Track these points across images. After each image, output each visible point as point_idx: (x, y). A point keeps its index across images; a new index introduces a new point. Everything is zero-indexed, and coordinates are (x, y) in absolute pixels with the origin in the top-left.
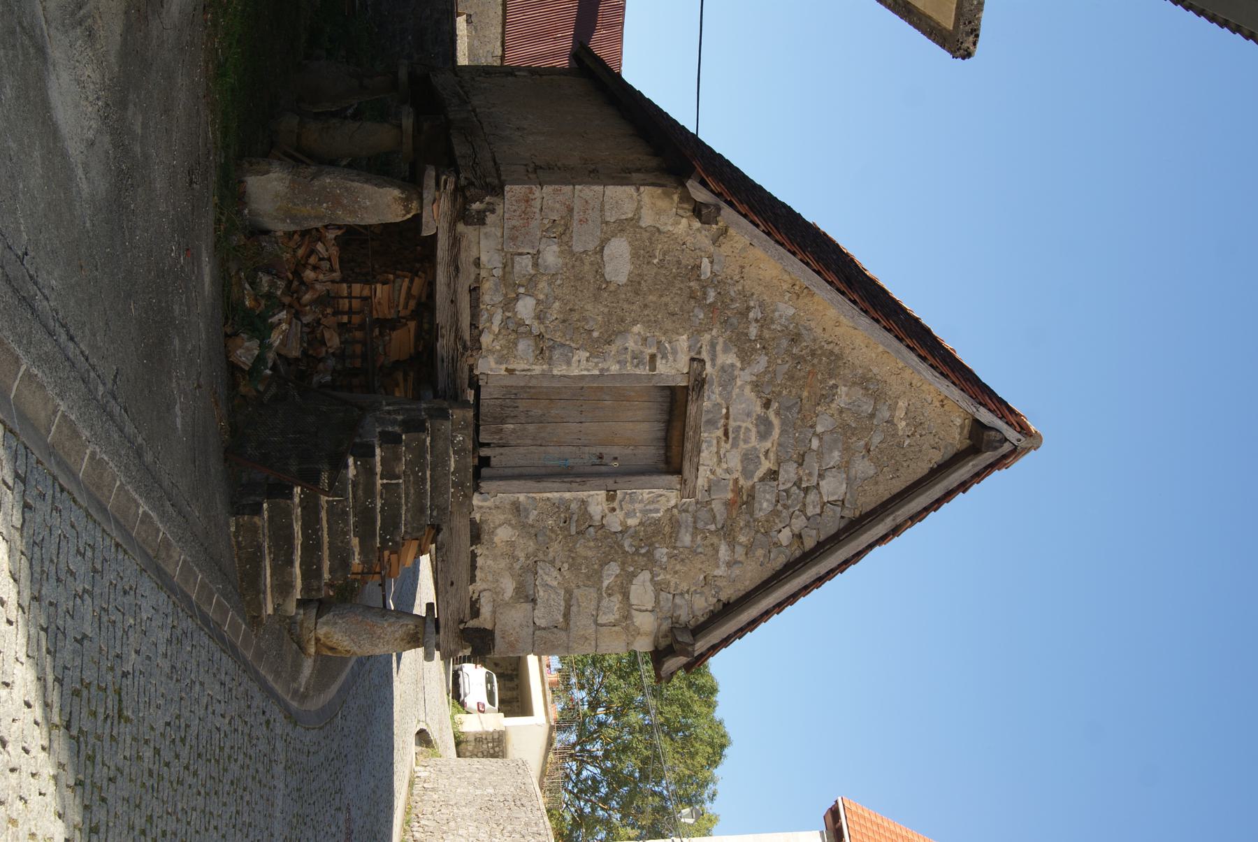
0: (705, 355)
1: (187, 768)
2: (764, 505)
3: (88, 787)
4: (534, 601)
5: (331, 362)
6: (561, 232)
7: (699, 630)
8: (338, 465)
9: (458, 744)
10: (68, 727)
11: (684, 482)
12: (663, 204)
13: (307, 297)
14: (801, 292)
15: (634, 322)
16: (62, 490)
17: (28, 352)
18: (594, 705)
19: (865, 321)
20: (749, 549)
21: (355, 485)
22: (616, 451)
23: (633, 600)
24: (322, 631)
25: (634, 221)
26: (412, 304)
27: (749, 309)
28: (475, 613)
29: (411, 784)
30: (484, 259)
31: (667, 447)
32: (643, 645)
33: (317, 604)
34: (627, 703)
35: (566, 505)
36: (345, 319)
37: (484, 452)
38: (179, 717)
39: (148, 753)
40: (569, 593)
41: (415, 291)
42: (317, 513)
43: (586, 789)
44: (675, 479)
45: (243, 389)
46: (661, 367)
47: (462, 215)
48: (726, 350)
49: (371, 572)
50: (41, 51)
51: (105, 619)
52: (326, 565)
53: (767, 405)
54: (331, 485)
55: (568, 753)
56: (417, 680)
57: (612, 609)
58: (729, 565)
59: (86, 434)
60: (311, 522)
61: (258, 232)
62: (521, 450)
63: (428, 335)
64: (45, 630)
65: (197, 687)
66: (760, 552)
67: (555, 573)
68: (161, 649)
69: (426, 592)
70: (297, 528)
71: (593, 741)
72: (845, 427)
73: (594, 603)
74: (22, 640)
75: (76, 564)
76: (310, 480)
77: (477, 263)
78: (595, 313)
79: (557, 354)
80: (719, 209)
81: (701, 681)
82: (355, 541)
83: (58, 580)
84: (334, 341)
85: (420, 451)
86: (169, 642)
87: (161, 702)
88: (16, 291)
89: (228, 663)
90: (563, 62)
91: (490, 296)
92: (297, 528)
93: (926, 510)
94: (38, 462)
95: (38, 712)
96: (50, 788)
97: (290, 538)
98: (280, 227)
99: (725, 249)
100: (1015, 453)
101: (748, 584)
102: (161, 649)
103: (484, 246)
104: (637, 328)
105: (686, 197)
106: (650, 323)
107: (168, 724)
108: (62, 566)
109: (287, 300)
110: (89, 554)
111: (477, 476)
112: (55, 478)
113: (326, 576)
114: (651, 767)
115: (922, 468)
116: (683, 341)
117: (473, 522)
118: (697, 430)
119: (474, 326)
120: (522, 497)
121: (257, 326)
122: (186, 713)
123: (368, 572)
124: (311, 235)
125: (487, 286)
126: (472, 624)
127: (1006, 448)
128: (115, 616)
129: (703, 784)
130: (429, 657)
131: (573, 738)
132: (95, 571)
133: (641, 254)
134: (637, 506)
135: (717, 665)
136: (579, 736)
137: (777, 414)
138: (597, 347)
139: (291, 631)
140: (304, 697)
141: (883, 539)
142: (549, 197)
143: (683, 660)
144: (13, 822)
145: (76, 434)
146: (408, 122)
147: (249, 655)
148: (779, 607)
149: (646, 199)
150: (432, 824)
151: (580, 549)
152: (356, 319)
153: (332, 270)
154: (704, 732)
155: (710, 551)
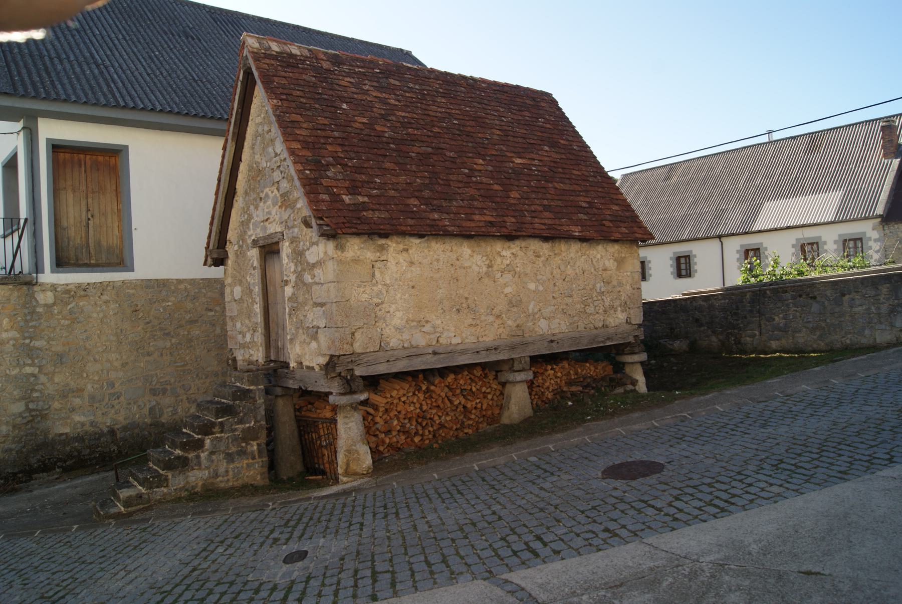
35: (290, 310)
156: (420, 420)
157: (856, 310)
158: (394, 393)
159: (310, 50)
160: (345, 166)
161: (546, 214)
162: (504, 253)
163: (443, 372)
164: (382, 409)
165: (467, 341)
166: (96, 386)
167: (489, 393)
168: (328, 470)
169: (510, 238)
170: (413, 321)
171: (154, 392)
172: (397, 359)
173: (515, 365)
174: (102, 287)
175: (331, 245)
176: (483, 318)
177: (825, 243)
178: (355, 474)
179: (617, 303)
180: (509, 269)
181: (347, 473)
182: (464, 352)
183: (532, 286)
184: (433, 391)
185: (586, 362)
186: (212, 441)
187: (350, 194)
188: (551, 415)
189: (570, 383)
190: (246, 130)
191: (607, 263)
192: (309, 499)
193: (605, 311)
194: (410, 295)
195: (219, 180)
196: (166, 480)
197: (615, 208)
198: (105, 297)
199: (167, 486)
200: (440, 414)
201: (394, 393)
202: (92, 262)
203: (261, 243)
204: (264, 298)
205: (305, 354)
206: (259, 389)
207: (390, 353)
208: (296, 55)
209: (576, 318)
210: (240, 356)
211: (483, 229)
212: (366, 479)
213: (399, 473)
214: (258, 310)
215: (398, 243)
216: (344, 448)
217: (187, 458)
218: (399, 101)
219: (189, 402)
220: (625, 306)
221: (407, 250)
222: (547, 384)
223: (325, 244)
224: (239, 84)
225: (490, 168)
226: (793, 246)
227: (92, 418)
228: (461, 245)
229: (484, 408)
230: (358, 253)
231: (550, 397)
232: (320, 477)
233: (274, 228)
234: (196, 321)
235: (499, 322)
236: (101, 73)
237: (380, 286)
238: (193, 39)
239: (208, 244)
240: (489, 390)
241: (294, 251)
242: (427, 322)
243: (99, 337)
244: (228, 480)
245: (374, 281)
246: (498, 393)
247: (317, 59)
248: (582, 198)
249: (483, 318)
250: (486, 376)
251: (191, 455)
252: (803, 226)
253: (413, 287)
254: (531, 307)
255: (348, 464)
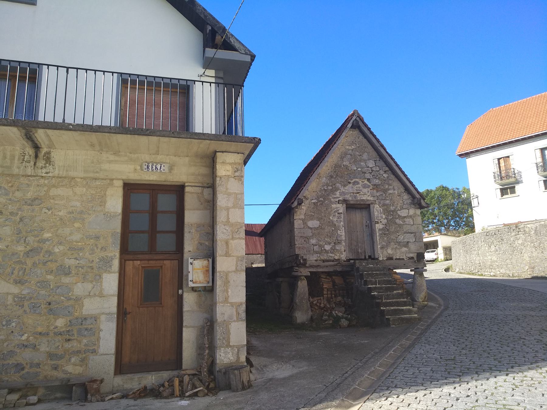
0: (337, 200)
1: (466, 340)
2: (377, 181)
3: (479, 370)
4: (408, 242)
5: (345, 299)
6: (307, 239)
7: (413, 197)
8: (374, 297)
9: (448, 260)
10: (460, 376)
11: (372, 203)
12: (298, 213)
13: (328, 306)
14: (319, 177)
15: (330, 219)
16: (389, 376)
17: (352, 385)
18: (433, 223)
19: (326, 159)
20: (389, 185)
21: (379, 293)
22: (364, 222)
23: (406, 215)
24: (420, 300)
25: (303, 220)
26: (328, 277)
27: (324, 189)
28: (412, 258)
29: (461, 273)
30: (315, 259)
31: (363, 208)
32: (418, 212)
33: (413, 301)
34: (432, 214)
35: (380, 234)
36: (333, 295)
37: (367, 257)
38: (451, 342)
39: (464, 351)
40: (405, 233)
41: (324, 277)
42: (388, 302)
43: (458, 224)
44: (371, 206)
45: (355, 323)
46: (341, 211)
47: (304, 265)
48: (335, 195)
49: (403, 287)
50: (271, 380)
51: (425, 364)
52: (402, 300)
53: (350, 183)
54: (380, 299)
55: (447, 229)
56: (433, 272)
57: (409, 221)
58: (394, 190)
59: (373, 369)
60: (391, 304)
61: (312, 319)
62: (366, 247)
63: (336, 273)
64: (431, 382)
65: (442, 336)
66: (390, 182)
67: (400, 237)
68: (432, 347)
69: (407, 271)
70: (392, 308)
71: (443, 223)
72: (354, 162)
73: (408, 226)
74: (436, 389)
75: (411, 372)
76: (379, 305)
77: (316, 260)
78: (327, 229)
79: (339, 239)
80: (299, 199)
81: (425, 194)
82: (395, 292)
83: (416, 378)
84: (339, 299)
85: (369, 275)
86: (429, 345)
87: (447, 347)
88: (336, 389)
89: (433, 327)
90: (262, 239)
91: (325, 257)
92: (392, 308)
93: (376, 138)
94: (382, 383)
95: (457, 385)
96: (480, 382)
97: (395, 310)
98: (310, 313)
99: (309, 196)
100: (359, 116)
101: (399, 185)
102: (432, 347)
103: (312, 259)
104: (331, 218)
105: (296, 207)
106: (330, 214)
107: (454, 345)
108: (412, 376)
109: (329, 311)
110: (407, 368)
111: (374, 259)
112: (387, 378)
113: (405, 300)
114: (450, 206)
115: (365, 140)
116: (334, 206)
117: (387, 260)
118: (357, 201)
119: (333, 261)
120: (379, 247)
121: (337, 319)
122: (450, 340)
123: (402, 288)
124: (312, 305)
125: (322, 258)
126: (416, 259)
127: (358, 119)
128: (424, 361)
129: (454, 191)
130: (426, 270)
131: (443, 228)
132: (412, 366)
133: (312, 218)
134: (379, 215)
135: (421, 190)
136: (442, 226)
137: (352, 180)
138: (337, 228)
139: (422, 309)
140: (439, 304)
141: (385, 149)
142: (298, 242)
143: (422, 201)
144: (492, 394)
145: (373, 371)
146: (281, 279)
147: (430, 321)
148: (405, 176)
149: (297, 217)
150: (473, 267)
151: (393, 230)
152: (333, 292)
153: (320, 299)
154: (438, 193)
155: (391, 195)
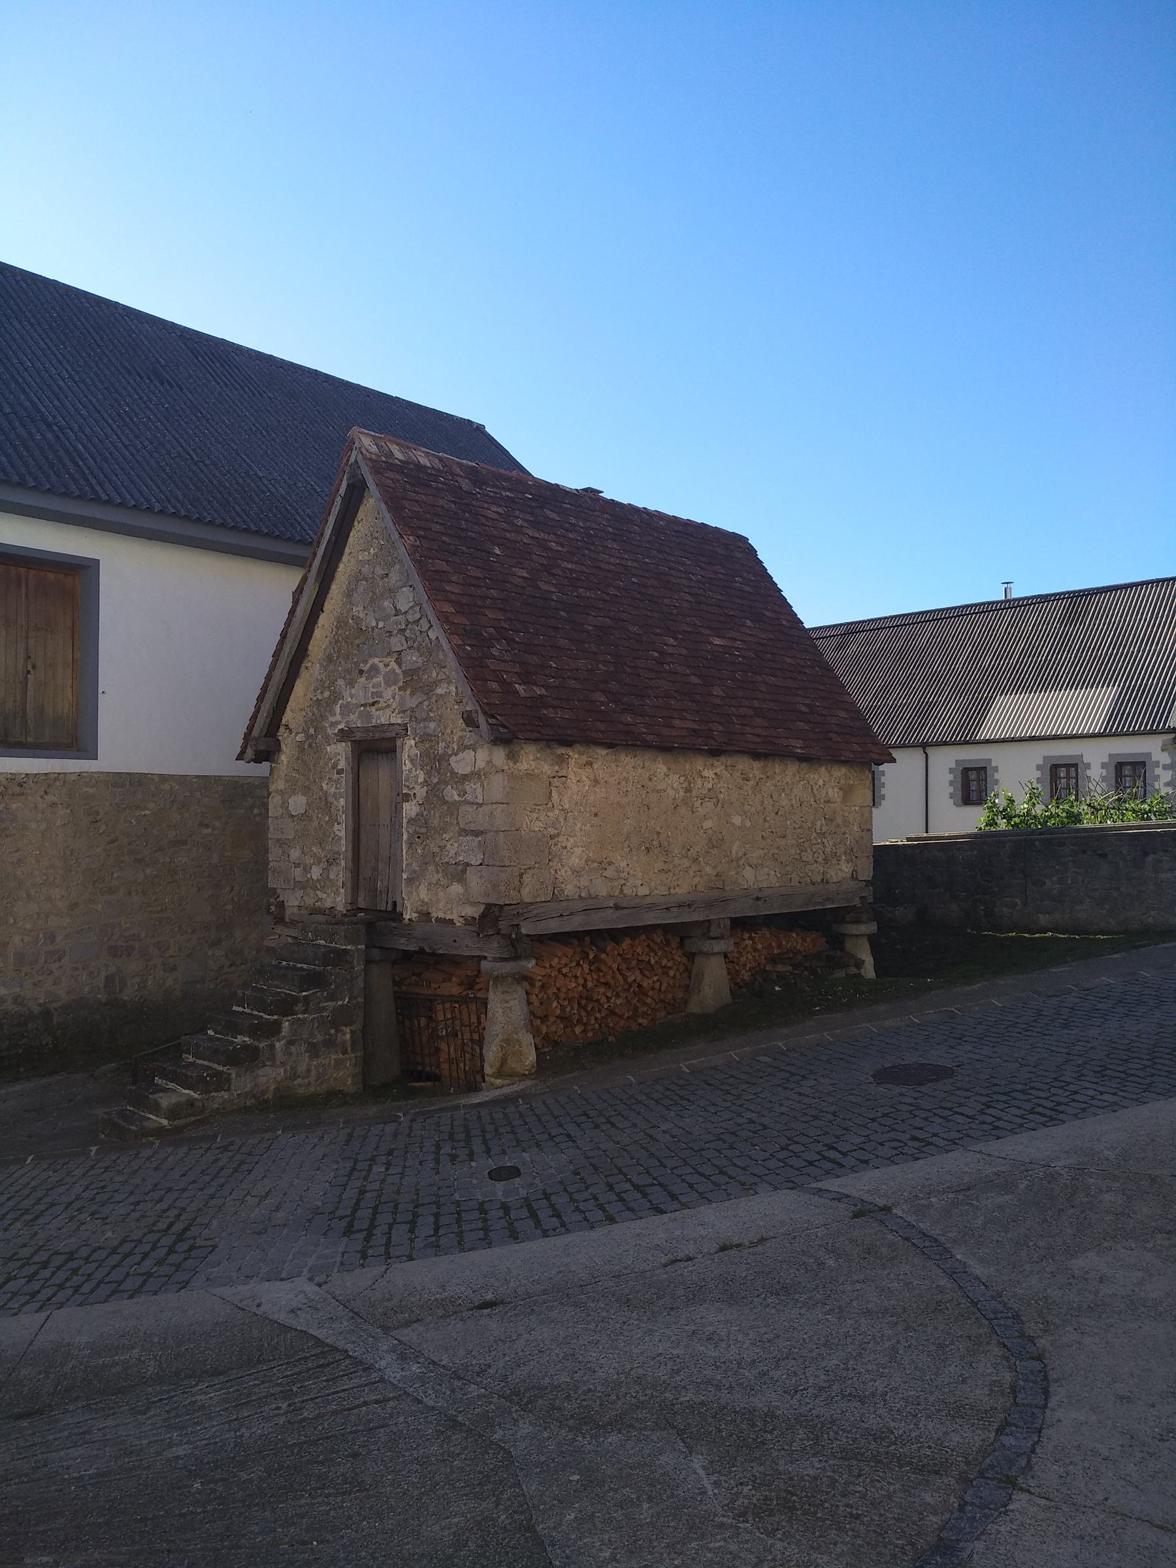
35: (410, 836)
46: (342, 765)
104: (325, 787)
156: (583, 1002)
157: (1163, 876)
158: (555, 962)
159: (441, 460)
160: (510, 641)
161: (759, 721)
162: (706, 773)
163: (615, 935)
164: (538, 984)
165: (655, 892)
166: (26, 939)
167: (670, 968)
168: (446, 1073)
169: (715, 753)
170: (593, 861)
171: (114, 951)
172: (571, 914)
173: (713, 929)
174: (48, 781)
175: (499, 756)
176: (677, 861)
177: (1088, 766)
178: (512, 1075)
179: (841, 850)
180: (711, 795)
181: (499, 1074)
182: (651, 907)
183: (737, 820)
184: (603, 962)
185: (791, 931)
186: (292, 1024)
187: (524, 683)
188: (758, 1003)
189: (773, 960)
190: (337, 567)
191: (830, 791)
192: (457, 1108)
193: (826, 860)
194: (592, 826)
195: (284, 635)
196: (228, 1080)
197: (842, 714)
198: (50, 798)
199: (229, 1089)
200: (609, 994)
201: (555, 962)
202: (30, 740)
203: (358, 736)
204: (353, 816)
205: (438, 901)
206: (358, 950)
207: (564, 904)
208: (425, 467)
209: (788, 868)
210: (293, 901)
211: (687, 740)
212: (529, 1083)
213: (575, 1074)
214: (343, 834)
215: (580, 753)
216: (501, 1037)
217: (256, 1048)
218: (562, 545)
219: (164, 970)
220: (851, 853)
221: (590, 764)
222: (743, 959)
223: (490, 750)
224: (339, 500)
225: (684, 652)
226: (1039, 768)
227: (18, 989)
228: (655, 761)
229: (663, 989)
230: (533, 764)
231: (746, 978)
232: (429, 1084)
233: (383, 717)
234: (184, 842)
235: (695, 868)
236: (58, 438)
237: (557, 812)
238: (172, 386)
239: (250, 728)
240: (670, 964)
241: (425, 754)
242: (610, 863)
243: (37, 861)
244: (309, 1083)
245: (550, 805)
246: (682, 968)
247: (452, 474)
248: (800, 699)
249: (677, 861)
250: (668, 943)
251: (262, 1045)
252: (1056, 738)
253: (596, 815)
254: (735, 848)
255: (504, 1061)
